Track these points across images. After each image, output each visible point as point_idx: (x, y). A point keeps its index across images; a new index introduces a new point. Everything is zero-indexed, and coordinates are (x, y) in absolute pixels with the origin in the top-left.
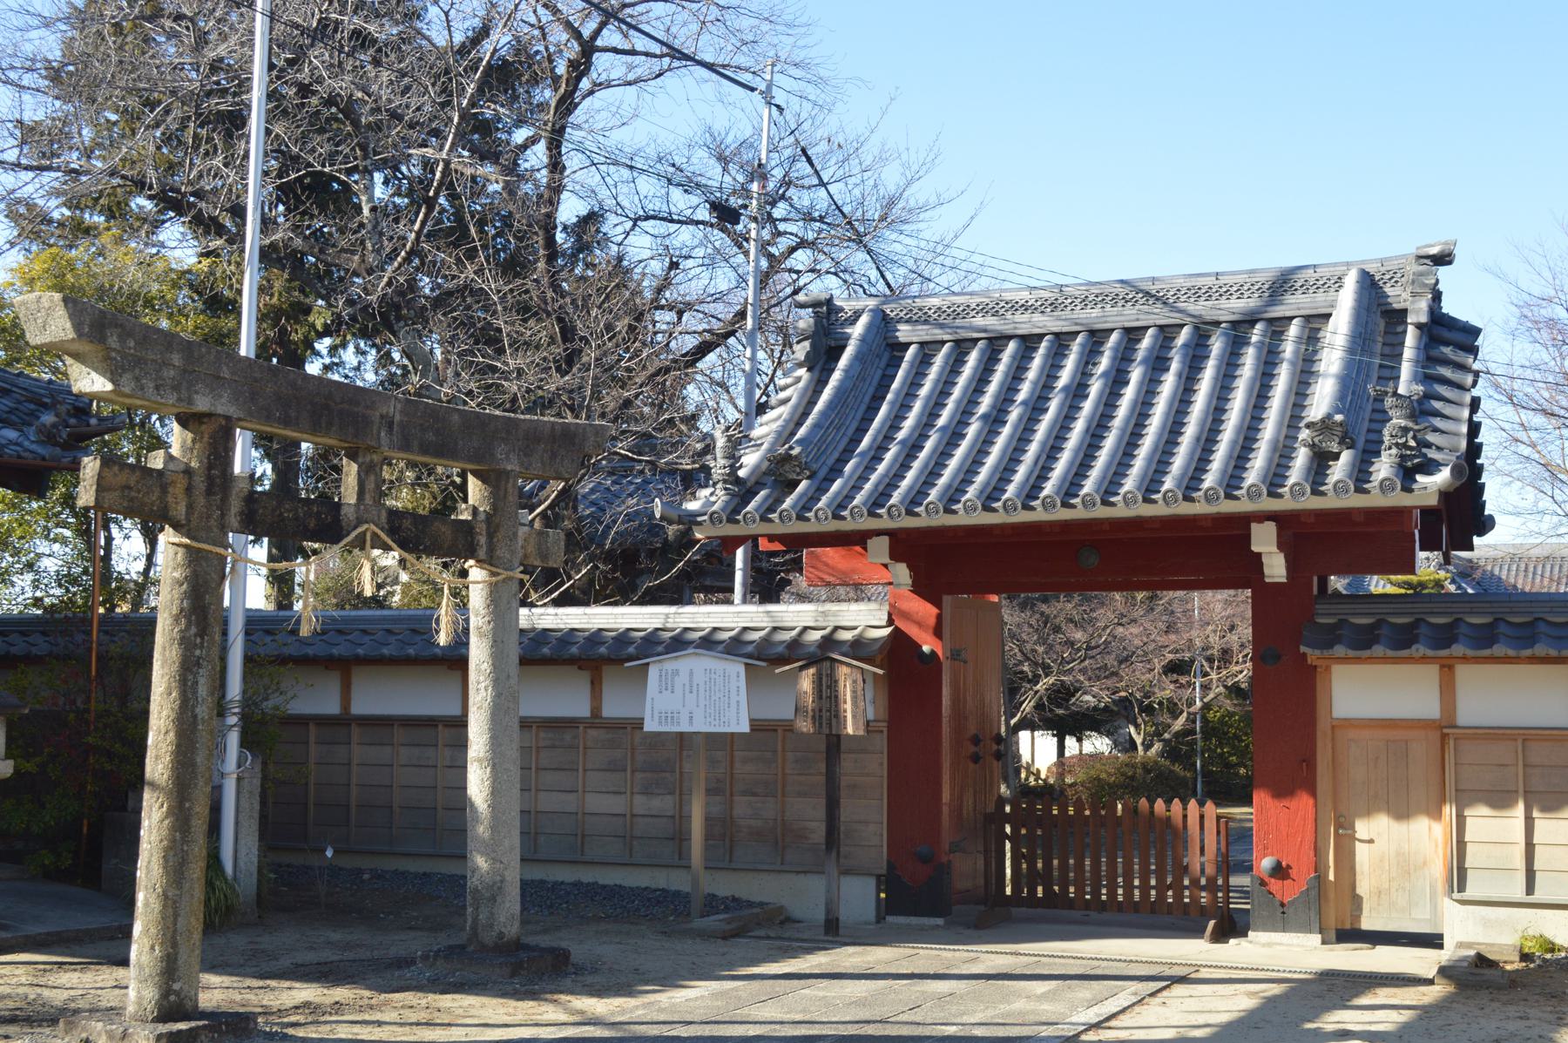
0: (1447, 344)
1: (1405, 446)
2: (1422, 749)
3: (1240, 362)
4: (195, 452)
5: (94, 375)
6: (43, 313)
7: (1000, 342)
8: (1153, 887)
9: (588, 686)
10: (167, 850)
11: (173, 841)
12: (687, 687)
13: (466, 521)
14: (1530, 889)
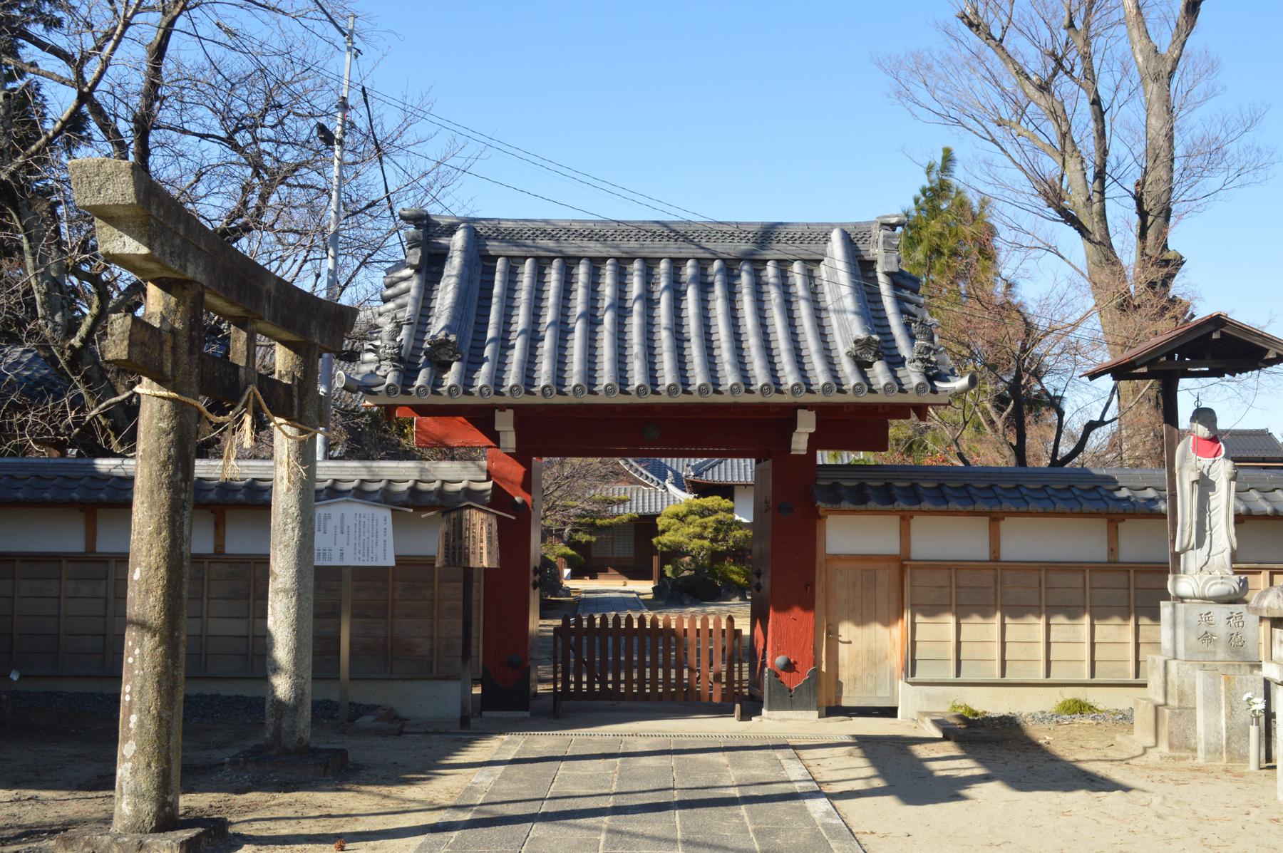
0: (907, 289)
1: (928, 361)
2: (886, 577)
3: (544, 288)
4: (179, 315)
5: (126, 238)
6: (103, 177)
7: (572, 261)
8: (610, 682)
9: (213, 526)
10: (160, 675)
11: (165, 667)
12: (339, 530)
13: (286, 384)
14: (958, 674)
